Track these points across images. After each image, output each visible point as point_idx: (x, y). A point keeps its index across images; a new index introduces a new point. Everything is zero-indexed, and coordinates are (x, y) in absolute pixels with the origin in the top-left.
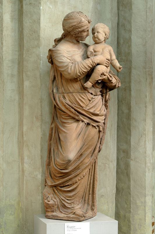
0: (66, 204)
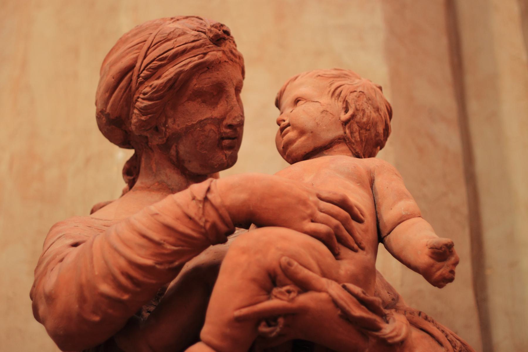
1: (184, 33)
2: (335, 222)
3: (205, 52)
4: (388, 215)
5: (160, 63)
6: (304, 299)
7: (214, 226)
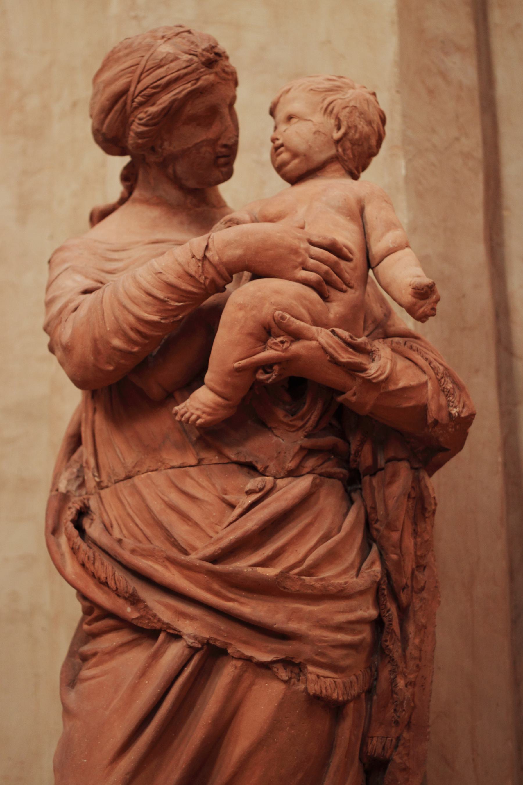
1: (176, 59)
2: (325, 268)
3: (197, 77)
4: (377, 247)
6: (296, 347)
7: (213, 281)
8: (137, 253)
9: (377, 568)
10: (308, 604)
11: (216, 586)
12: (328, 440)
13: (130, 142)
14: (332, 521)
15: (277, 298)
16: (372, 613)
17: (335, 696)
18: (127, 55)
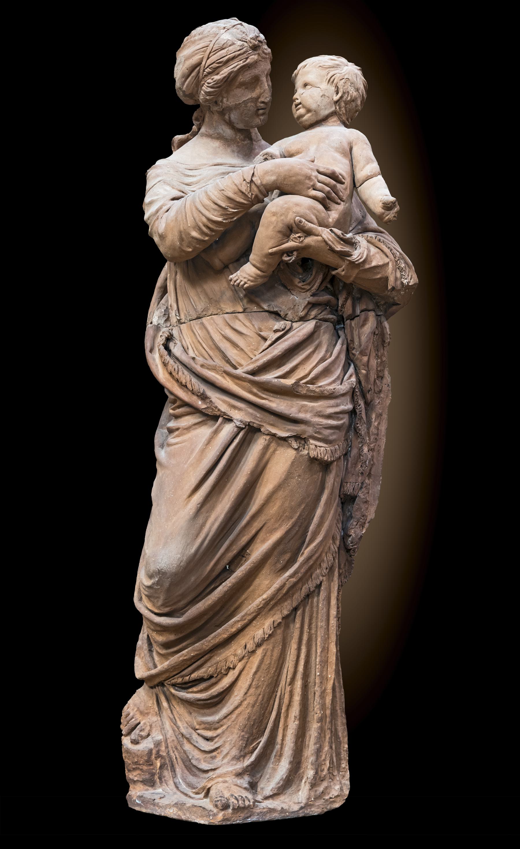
0: (195, 754)
2: (328, 189)
4: (360, 175)
5: (218, 65)
6: (310, 240)
7: (256, 196)
8: (207, 172)
9: (353, 379)
10: (311, 402)
11: (255, 390)
12: (326, 297)
13: (201, 97)
14: (327, 352)
15: (297, 209)
16: (349, 406)
17: (326, 458)
18: (201, 39)
